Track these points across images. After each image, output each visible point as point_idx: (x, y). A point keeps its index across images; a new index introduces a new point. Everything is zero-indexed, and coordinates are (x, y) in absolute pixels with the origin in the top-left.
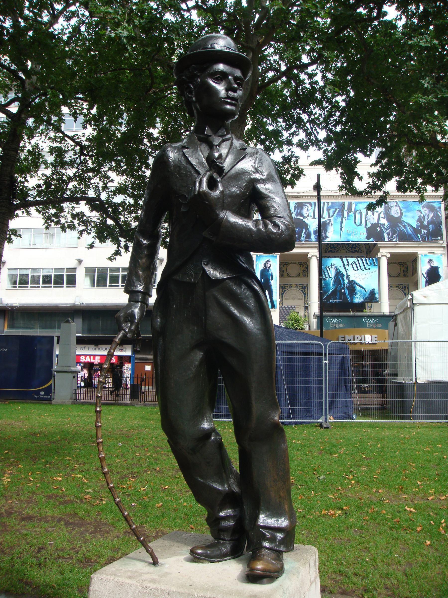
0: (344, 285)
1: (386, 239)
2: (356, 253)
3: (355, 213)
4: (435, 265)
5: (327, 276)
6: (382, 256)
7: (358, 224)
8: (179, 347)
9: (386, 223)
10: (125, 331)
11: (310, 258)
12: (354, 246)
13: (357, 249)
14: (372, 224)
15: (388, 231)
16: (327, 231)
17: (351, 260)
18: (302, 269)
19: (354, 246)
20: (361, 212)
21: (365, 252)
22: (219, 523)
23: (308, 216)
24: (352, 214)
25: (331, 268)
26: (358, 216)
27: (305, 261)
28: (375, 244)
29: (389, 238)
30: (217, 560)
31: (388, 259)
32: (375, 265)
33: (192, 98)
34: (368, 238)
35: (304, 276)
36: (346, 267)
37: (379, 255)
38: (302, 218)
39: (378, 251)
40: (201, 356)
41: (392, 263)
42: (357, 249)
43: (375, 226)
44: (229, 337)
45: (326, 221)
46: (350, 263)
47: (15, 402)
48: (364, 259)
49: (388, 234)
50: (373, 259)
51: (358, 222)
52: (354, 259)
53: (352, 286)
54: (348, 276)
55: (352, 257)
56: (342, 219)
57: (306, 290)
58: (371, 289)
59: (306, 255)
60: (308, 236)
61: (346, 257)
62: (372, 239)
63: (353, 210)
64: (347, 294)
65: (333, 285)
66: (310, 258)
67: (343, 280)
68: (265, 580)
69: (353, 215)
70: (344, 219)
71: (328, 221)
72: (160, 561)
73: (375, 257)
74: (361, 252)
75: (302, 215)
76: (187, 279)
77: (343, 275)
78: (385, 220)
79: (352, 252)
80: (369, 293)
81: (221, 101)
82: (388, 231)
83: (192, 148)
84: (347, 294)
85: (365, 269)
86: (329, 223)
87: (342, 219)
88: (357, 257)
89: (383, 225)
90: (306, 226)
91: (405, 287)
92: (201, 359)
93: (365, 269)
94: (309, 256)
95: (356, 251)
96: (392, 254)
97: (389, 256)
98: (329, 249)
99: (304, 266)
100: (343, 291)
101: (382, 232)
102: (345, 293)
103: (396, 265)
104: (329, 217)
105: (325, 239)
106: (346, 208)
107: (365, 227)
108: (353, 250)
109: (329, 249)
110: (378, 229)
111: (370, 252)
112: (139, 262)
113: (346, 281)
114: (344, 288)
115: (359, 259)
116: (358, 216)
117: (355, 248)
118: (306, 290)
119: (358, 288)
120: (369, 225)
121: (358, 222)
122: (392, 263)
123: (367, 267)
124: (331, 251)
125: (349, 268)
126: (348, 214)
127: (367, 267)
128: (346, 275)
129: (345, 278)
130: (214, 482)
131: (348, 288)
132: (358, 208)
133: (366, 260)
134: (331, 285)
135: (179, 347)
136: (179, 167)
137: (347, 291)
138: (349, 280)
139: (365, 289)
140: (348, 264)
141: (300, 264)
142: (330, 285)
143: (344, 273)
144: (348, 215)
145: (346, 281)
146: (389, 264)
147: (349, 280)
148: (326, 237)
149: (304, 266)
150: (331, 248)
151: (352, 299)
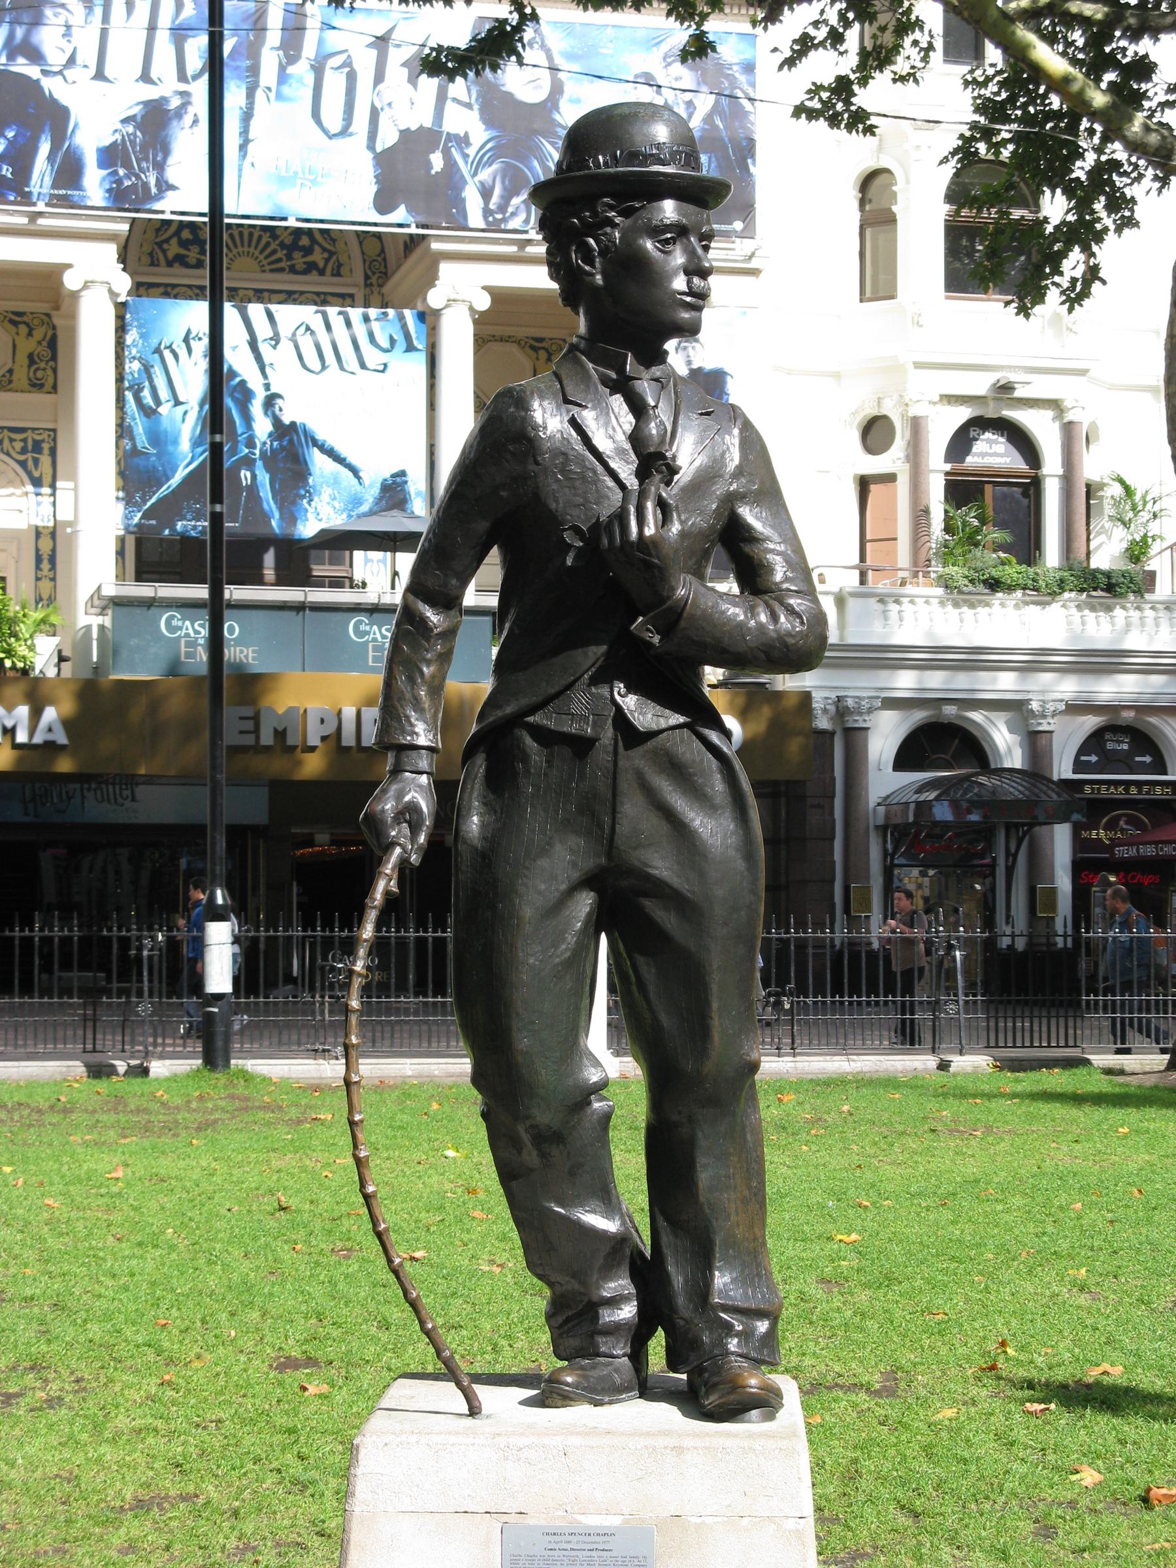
0: (251, 443)
1: (475, 219)
2: (314, 276)
3: (318, 70)
4: (709, 365)
5: (164, 393)
6: (451, 302)
7: (335, 125)
8: (543, 887)
9: (480, 135)
10: (403, 847)
11: (75, 296)
12: (305, 241)
13: (318, 257)
14: (405, 134)
15: (485, 175)
16: (166, 152)
17: (290, 315)
18: (27, 346)
19: (305, 241)
20: (348, 63)
21: (359, 277)
22: (596, 1317)
23: (71, 61)
24: (301, 70)
25: (182, 351)
26: (334, 83)
27: (43, 307)
28: (413, 243)
29: (487, 212)
30: (607, 1399)
31: (481, 320)
32: (410, 348)
33: (593, 275)
34: (383, 203)
35: (36, 386)
36: (264, 348)
37: (435, 298)
38: (33, 72)
39: (430, 279)
40: (588, 910)
41: (494, 339)
42: (318, 257)
43: (416, 142)
44: (662, 865)
45: (164, 100)
46: (285, 331)
47: (288, 1025)
48: (355, 313)
49: (486, 193)
50: (401, 318)
51: (333, 116)
52: (307, 313)
53: (291, 450)
54: (270, 402)
55: (291, 297)
56: (251, 95)
57: (45, 460)
58: (386, 472)
59: (51, 275)
60: (69, 172)
61: (260, 296)
62: (400, 214)
63: (309, 49)
64: (266, 493)
65: (196, 443)
66: (75, 296)
67: (248, 419)
68: (754, 1413)
69: (310, 78)
70: (259, 95)
71: (175, 103)
72: (485, 1409)
73: (409, 305)
74: (337, 273)
75: (35, 55)
76: (573, 728)
77: (244, 394)
78: (475, 114)
79: (293, 270)
80: (376, 491)
81: (675, 301)
82: (485, 175)
83: (594, 408)
84: (266, 493)
85: (363, 366)
86: (180, 113)
87: (251, 95)
88: (321, 300)
89: (463, 141)
90: (56, 118)
91: (37, 447)
92: (589, 914)
93: (363, 366)
94: (71, 281)
95: (311, 267)
96: (500, 296)
97: (483, 303)
98: (174, 249)
99: (38, 334)
100: (245, 475)
101: (451, 180)
102: (253, 489)
103: (514, 349)
104: (182, 77)
105: (159, 197)
106: (273, 37)
107: (371, 146)
108: (299, 260)
109: (174, 249)
110: (437, 161)
111: (385, 276)
112: (422, 673)
113: (262, 427)
114: (248, 462)
115: (332, 311)
116: (334, 83)
117: (308, 251)
118: (45, 460)
119: (319, 462)
120: (388, 138)
121: (333, 116)
122: (494, 339)
123: (373, 357)
124: (181, 260)
125: (280, 358)
126: (282, 69)
127: (373, 357)
128: (260, 395)
129: (256, 408)
130: (593, 1212)
131: (270, 461)
132: (334, 41)
133: (366, 319)
134: (185, 445)
135: (543, 887)
136: (564, 454)
137: (264, 477)
138: (277, 422)
139: (355, 471)
140: (276, 339)
141: (16, 319)
142: (176, 442)
143: (255, 382)
144: (283, 77)
145: (262, 427)
146: (481, 342)
147: (277, 422)
148: (165, 186)
149: (38, 334)
150: (184, 244)
151: (291, 517)
